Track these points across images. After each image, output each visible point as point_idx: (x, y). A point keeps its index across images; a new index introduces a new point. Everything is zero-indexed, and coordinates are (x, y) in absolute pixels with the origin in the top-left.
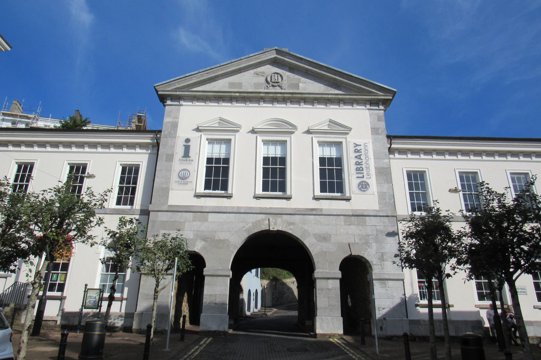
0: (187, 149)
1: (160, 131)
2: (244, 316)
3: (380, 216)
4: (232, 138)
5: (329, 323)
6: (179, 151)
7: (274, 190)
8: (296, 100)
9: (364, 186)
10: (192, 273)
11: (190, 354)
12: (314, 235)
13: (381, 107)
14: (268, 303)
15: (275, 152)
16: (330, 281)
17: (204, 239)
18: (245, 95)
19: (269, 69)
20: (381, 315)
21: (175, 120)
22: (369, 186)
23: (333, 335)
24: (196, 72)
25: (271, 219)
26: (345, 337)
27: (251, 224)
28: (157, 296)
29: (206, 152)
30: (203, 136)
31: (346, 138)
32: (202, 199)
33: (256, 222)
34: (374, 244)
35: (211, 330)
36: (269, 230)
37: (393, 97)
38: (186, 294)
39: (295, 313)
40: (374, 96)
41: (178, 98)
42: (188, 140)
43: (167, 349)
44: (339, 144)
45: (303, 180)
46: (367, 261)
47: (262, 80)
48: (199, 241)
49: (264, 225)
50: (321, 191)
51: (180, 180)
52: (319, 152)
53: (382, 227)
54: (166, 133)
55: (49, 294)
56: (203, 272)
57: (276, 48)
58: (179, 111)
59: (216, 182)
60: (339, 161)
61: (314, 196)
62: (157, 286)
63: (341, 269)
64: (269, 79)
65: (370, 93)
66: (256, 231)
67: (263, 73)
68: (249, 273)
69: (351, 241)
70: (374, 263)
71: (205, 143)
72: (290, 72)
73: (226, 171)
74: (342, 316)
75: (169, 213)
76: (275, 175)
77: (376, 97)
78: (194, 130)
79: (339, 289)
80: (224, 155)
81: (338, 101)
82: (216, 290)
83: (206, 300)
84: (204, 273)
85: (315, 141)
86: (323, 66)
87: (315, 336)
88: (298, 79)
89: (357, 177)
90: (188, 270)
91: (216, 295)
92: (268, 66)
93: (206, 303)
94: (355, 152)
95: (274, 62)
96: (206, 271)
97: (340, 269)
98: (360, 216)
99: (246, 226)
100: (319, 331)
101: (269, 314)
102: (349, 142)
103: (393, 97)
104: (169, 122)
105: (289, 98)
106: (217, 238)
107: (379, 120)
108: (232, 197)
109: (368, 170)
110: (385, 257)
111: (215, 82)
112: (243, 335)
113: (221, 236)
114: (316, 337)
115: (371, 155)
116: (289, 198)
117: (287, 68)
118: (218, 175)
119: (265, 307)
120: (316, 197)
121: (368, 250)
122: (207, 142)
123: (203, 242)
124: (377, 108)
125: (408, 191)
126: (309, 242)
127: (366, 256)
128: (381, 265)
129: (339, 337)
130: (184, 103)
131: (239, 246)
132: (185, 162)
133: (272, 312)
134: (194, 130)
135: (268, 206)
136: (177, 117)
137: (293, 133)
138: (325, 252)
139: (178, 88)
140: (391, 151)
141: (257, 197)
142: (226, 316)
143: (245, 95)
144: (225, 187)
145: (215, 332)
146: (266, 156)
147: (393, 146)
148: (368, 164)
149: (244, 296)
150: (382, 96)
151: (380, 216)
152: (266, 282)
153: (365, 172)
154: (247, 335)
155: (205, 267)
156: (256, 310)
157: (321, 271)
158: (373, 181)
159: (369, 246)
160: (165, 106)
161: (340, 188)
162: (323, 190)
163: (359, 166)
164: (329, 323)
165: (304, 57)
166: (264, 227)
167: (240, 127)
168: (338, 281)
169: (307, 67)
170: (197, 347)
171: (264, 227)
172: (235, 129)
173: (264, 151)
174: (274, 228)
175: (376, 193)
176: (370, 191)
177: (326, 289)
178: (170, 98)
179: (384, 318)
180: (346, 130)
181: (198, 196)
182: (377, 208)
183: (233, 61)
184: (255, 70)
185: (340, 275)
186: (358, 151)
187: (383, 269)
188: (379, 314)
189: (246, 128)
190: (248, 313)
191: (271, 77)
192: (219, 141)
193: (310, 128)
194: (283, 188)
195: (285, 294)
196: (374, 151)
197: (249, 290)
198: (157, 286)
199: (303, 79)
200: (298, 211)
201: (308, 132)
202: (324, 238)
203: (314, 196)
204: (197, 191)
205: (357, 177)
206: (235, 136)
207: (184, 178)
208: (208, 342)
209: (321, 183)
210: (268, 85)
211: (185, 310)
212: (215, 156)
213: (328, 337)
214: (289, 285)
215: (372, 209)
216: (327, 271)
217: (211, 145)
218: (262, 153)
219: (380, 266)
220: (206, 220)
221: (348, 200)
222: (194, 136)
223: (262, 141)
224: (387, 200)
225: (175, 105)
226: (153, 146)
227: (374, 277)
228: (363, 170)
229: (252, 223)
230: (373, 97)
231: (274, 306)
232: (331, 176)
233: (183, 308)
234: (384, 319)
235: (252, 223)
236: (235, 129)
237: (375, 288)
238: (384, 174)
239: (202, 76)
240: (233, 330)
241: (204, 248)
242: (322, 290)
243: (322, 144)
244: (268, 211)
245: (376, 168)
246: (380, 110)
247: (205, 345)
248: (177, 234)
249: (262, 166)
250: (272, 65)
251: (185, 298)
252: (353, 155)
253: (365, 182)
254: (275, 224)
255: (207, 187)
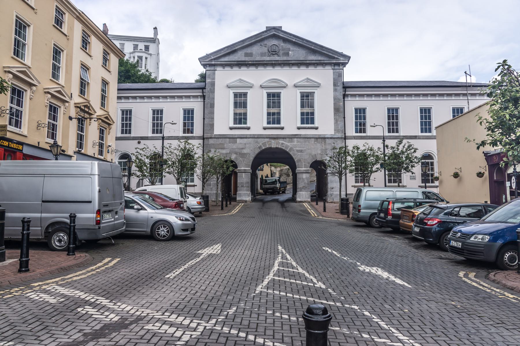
36: (270, 148)
37: (349, 61)
55: (188, 184)
64: (270, 50)
65: (334, 58)
98: (323, 138)
105: (282, 64)
147: (347, 93)
208: (111, 264)
244: (271, 137)
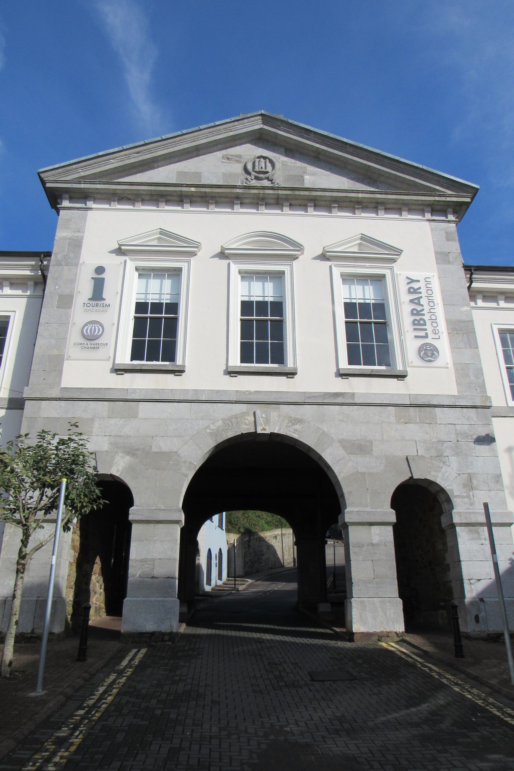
0: (98, 286)
1: (48, 254)
2: (201, 593)
3: (462, 407)
4: (184, 266)
5: (376, 611)
6: (84, 288)
7: (262, 359)
8: (299, 202)
9: (428, 353)
10: (107, 517)
11: (91, 702)
12: (341, 441)
13: (451, 217)
14: (240, 571)
15: (263, 292)
16: (375, 529)
17: (131, 452)
18: (208, 190)
19: (250, 151)
20: (474, 594)
21: (78, 234)
22: (438, 352)
23: (387, 635)
24: (116, 149)
25: (258, 413)
26: (408, 638)
27: (220, 423)
28: (24, 565)
29: (135, 290)
30: (129, 262)
31: (391, 269)
32: (127, 376)
33: (230, 419)
34: (453, 459)
35: (144, 630)
36: (255, 434)
37: (472, 199)
38: (98, 560)
39: (293, 586)
40: (440, 196)
41: (82, 196)
42: (100, 270)
43: (40, 692)
44: (379, 279)
45: (316, 343)
46: (442, 490)
47: (238, 168)
48: (121, 454)
49: (246, 424)
50: (350, 363)
51: (86, 342)
52: (344, 294)
53: (466, 428)
54: (59, 257)
56: (127, 514)
57: (263, 112)
58: (85, 219)
59: (154, 347)
60: (381, 308)
61: (338, 370)
62: (25, 542)
63: (393, 506)
64: (250, 167)
65: (431, 192)
66: (231, 434)
67: (240, 156)
68: (208, 522)
69: (411, 452)
70: (456, 493)
71: (132, 275)
72: (287, 155)
73: (172, 326)
74: (401, 596)
75: (63, 403)
76: (263, 334)
77: (443, 199)
78: (112, 252)
79: (393, 544)
80: (168, 297)
81: (374, 206)
82: (153, 551)
83: (135, 570)
84: (131, 518)
85: (337, 272)
86: (346, 144)
87: (350, 636)
88: (301, 167)
89: (416, 337)
90: (93, 508)
91: (153, 560)
92: (249, 146)
93: (134, 576)
94: (409, 292)
95: (259, 138)
96: (133, 514)
97: (393, 506)
98: (424, 405)
99: (212, 427)
100: (357, 627)
101: (241, 588)
102: (400, 273)
103: (472, 199)
104: (65, 238)
105: (287, 198)
106: (155, 449)
107: (448, 240)
108: (183, 371)
109: (435, 325)
110: (475, 482)
111: (151, 171)
112: (207, 635)
113: (164, 445)
114: (351, 640)
115: (438, 297)
116: (291, 374)
117: (283, 150)
118: (156, 335)
119: (235, 577)
120: (342, 372)
121: (443, 470)
122: (137, 274)
123: (128, 458)
124: (444, 218)
125: (503, 366)
126: (332, 456)
127: (439, 481)
128: (468, 497)
129: (398, 639)
130: (95, 206)
131: (198, 463)
132: (95, 308)
133: (247, 586)
134: (112, 252)
135: (253, 389)
136: (81, 230)
137: (295, 258)
138: (364, 474)
139: (83, 177)
140: (473, 294)
141: (231, 373)
142: (174, 603)
143: (208, 190)
144: (170, 354)
145: (152, 634)
146: (246, 299)
147: (474, 285)
148: (433, 314)
149: (202, 560)
150: (452, 197)
151: (462, 407)
152: (234, 538)
153: (429, 327)
154: (215, 635)
155: (132, 504)
156: (220, 583)
157: (356, 509)
158: (443, 344)
159: (444, 463)
160: (58, 211)
161: (385, 355)
162: (353, 359)
163: (418, 318)
164: (376, 611)
165: (312, 129)
166: (246, 428)
167: (197, 245)
168: (390, 529)
169: (318, 146)
170: (112, 677)
171: (246, 427)
172: (188, 249)
173: (241, 291)
174: (264, 429)
175: (451, 365)
176: (439, 362)
177: (368, 545)
178: (67, 196)
179: (480, 599)
180: (391, 254)
181: (119, 370)
182: (454, 392)
183: (185, 132)
184: (224, 152)
185: (393, 518)
186: (415, 291)
187: (472, 504)
188: (471, 591)
189: (209, 247)
190: (208, 588)
191: (254, 164)
192: (159, 273)
193: (324, 255)
194: (279, 356)
195: (263, 555)
196: (442, 292)
197: (210, 550)
198: (25, 542)
199: (310, 168)
200: (309, 398)
201: (324, 257)
202: (360, 448)
203: (338, 370)
204: (117, 362)
205: (416, 337)
206: (189, 262)
207: (92, 337)
208: (136, 662)
209: (350, 348)
210: (248, 177)
211: (98, 588)
212: (152, 299)
213: (375, 638)
214: (269, 542)
215: (446, 393)
216: (368, 509)
217: (144, 281)
218: (240, 294)
219: (466, 500)
220: (135, 416)
221: (401, 377)
222: (112, 263)
223: (240, 272)
224: (472, 378)
225: (78, 209)
226: (36, 284)
227: (456, 520)
228: (425, 324)
229: (223, 420)
230: (437, 198)
231: (247, 575)
232: (367, 335)
233: (91, 586)
234: (482, 600)
235: (223, 420)
236: (188, 249)
237: (460, 540)
238: (463, 332)
239: (128, 156)
240: (188, 625)
241: (130, 469)
242: (360, 546)
243: (348, 279)
245: (448, 322)
246: (449, 222)
247: (129, 672)
248: (71, 432)
249: (239, 317)
250: (255, 144)
251: (97, 567)
252: (405, 298)
253: (430, 345)
254: (267, 421)
255: (136, 355)
